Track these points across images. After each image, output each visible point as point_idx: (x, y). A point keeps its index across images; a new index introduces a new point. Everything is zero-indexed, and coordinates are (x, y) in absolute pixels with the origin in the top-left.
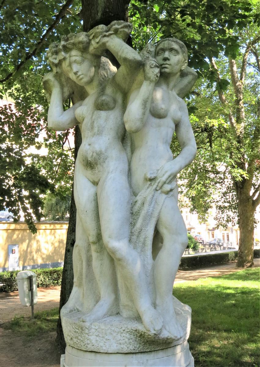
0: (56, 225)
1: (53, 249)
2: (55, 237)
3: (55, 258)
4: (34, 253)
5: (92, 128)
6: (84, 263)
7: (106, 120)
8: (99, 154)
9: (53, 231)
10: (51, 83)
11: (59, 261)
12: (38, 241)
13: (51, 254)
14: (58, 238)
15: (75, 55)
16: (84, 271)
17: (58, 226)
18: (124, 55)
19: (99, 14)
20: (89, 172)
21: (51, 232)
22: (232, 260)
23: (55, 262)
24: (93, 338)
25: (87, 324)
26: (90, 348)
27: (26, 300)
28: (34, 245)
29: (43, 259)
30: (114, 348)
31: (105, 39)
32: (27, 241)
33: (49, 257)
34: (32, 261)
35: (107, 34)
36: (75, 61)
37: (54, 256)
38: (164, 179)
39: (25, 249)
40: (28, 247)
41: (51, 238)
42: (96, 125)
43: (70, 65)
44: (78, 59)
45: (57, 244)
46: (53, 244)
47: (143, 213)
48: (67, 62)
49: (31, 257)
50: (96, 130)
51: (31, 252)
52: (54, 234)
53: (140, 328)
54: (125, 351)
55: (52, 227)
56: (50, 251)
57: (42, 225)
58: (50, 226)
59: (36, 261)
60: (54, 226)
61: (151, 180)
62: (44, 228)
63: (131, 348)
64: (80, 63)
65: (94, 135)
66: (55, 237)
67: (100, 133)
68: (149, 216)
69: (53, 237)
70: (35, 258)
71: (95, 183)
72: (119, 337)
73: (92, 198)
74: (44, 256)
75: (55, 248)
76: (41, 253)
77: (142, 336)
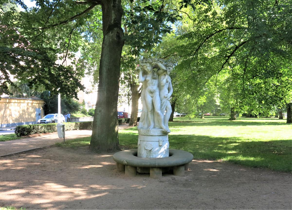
0: (21, 101)
1: (19, 115)
2: (20, 108)
3: (20, 120)
4: (8, 117)
5: (152, 84)
6: (146, 116)
7: (156, 82)
8: (154, 90)
9: (19, 104)
10: (140, 70)
11: (23, 122)
12: (10, 110)
13: (17, 118)
14: (22, 108)
15: (148, 64)
16: (146, 118)
17: (22, 101)
18: (163, 68)
19: (113, 21)
20: (151, 95)
21: (18, 105)
22: (124, 123)
23: (20, 122)
24: (152, 133)
25: (150, 130)
26: (151, 135)
27: (62, 135)
28: (8, 112)
29: (13, 120)
30: (157, 134)
31: (157, 63)
32: (4, 110)
33: (16, 120)
34: (6, 121)
35: (158, 61)
36: (148, 66)
37: (19, 119)
38: (169, 97)
39: (3, 114)
40: (4, 113)
41: (18, 108)
42: (153, 83)
43: (147, 67)
44: (149, 66)
45: (21, 112)
46: (19, 112)
47: (164, 105)
48: (146, 66)
49: (6, 119)
50: (153, 84)
51: (6, 116)
52: (19, 106)
53: (163, 130)
54: (159, 135)
55: (19, 101)
56: (17, 116)
57: (12, 100)
58: (18, 101)
59: (9, 121)
60: (24, 101)
61: (166, 97)
62: (14, 102)
63: (160, 134)
64: (149, 67)
65: (153, 85)
66: (20, 108)
67: (154, 85)
68: (165, 105)
69: (19, 107)
70: (8, 120)
71: (152, 97)
72: (158, 132)
73: (151, 100)
74: (14, 119)
75: (20, 114)
76: (12, 117)
77: (163, 132)
